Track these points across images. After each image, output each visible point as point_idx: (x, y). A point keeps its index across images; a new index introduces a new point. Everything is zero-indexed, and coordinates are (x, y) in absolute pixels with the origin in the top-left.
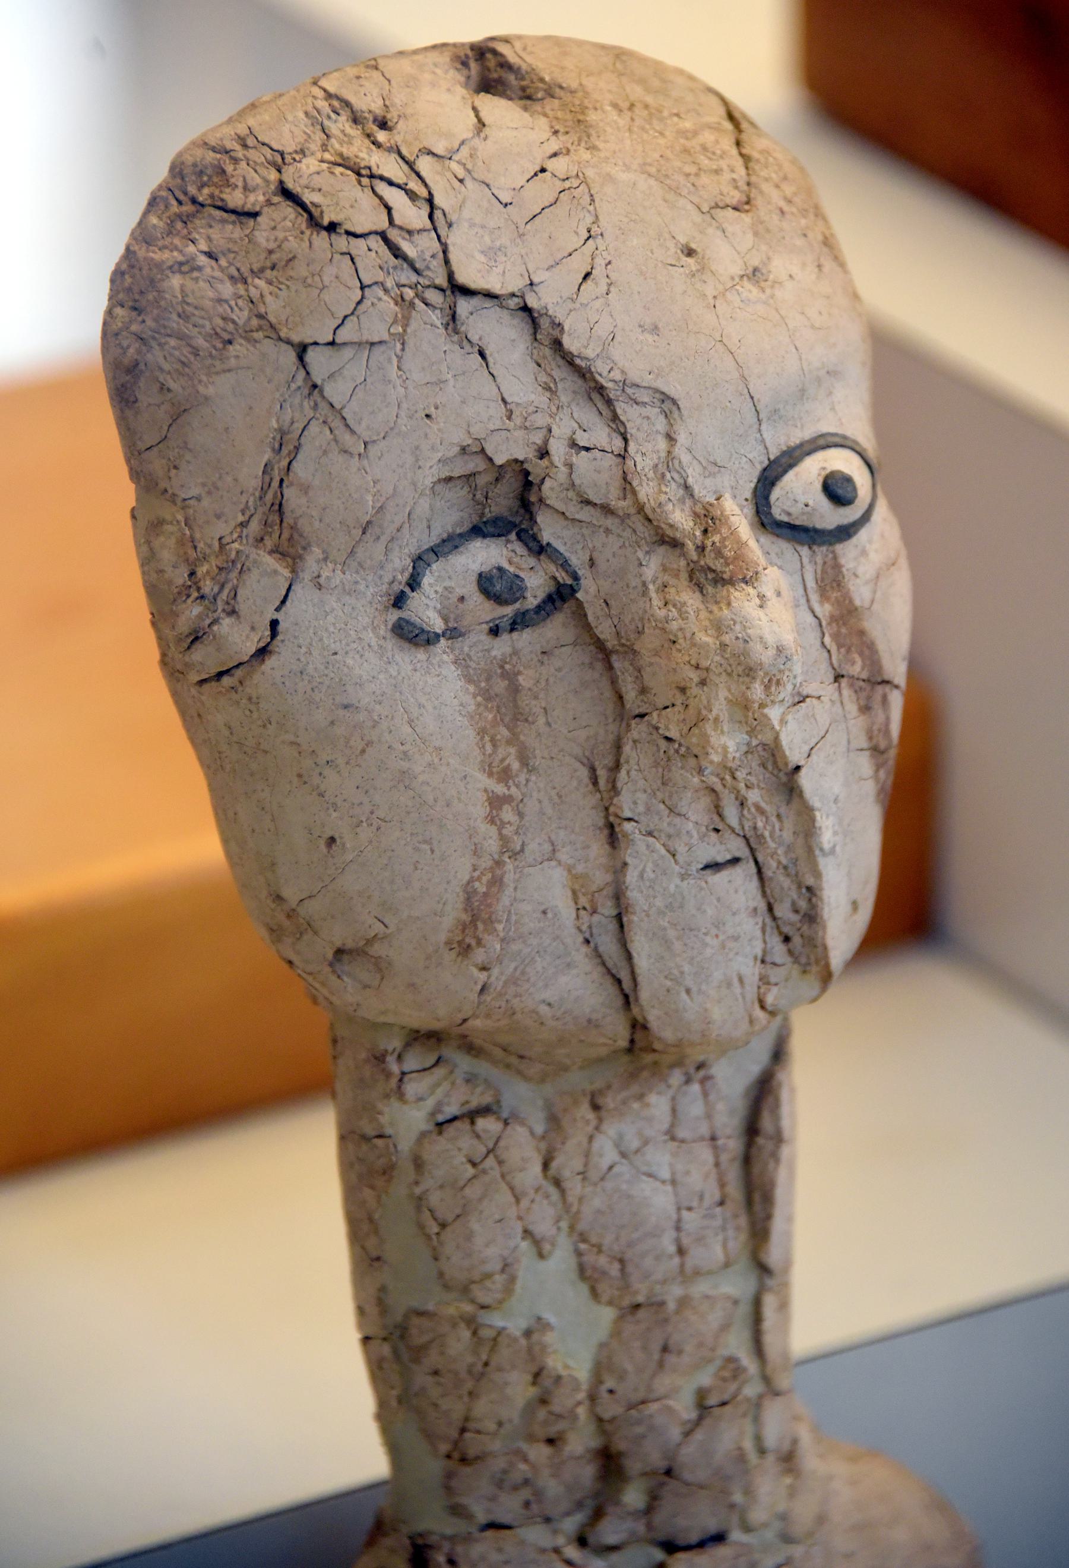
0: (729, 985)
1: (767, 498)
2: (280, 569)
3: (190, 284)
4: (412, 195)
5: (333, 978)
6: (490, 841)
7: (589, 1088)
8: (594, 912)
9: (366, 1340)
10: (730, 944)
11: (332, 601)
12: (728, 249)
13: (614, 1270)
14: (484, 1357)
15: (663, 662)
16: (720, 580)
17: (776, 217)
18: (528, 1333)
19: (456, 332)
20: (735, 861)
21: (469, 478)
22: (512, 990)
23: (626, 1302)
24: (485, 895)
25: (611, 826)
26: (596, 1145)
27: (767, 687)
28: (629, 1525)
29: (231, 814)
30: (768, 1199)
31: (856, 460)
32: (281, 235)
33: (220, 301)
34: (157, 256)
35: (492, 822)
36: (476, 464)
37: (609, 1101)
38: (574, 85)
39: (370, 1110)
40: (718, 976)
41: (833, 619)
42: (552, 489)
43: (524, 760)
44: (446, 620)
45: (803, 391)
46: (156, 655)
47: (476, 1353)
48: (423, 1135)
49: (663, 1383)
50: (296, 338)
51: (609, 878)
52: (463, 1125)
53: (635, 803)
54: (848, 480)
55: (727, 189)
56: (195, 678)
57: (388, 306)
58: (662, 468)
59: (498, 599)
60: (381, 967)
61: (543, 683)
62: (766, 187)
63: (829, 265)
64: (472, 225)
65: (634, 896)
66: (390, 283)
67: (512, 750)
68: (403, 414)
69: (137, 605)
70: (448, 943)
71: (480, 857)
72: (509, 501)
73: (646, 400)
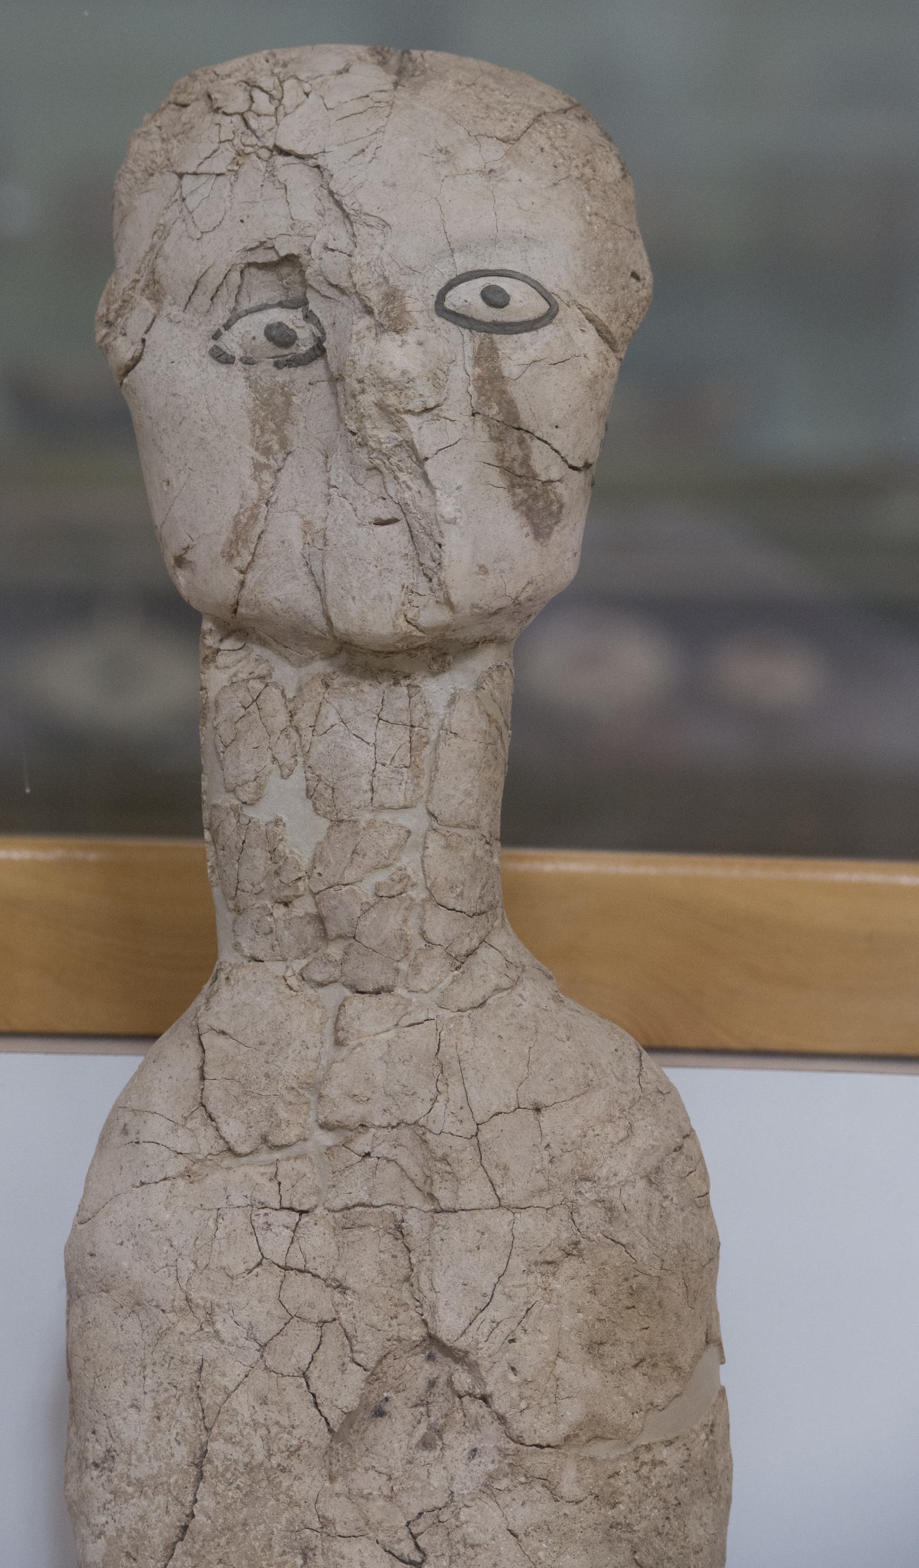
2: (150, 307)
6: (252, 491)
14: (243, 837)
24: (246, 524)
35: (255, 479)
37: (336, 683)
42: (311, 274)
50: (179, 171)
53: (338, 476)
61: (307, 402)
67: (275, 438)
68: (226, 218)
71: (245, 500)
73: (373, 224)
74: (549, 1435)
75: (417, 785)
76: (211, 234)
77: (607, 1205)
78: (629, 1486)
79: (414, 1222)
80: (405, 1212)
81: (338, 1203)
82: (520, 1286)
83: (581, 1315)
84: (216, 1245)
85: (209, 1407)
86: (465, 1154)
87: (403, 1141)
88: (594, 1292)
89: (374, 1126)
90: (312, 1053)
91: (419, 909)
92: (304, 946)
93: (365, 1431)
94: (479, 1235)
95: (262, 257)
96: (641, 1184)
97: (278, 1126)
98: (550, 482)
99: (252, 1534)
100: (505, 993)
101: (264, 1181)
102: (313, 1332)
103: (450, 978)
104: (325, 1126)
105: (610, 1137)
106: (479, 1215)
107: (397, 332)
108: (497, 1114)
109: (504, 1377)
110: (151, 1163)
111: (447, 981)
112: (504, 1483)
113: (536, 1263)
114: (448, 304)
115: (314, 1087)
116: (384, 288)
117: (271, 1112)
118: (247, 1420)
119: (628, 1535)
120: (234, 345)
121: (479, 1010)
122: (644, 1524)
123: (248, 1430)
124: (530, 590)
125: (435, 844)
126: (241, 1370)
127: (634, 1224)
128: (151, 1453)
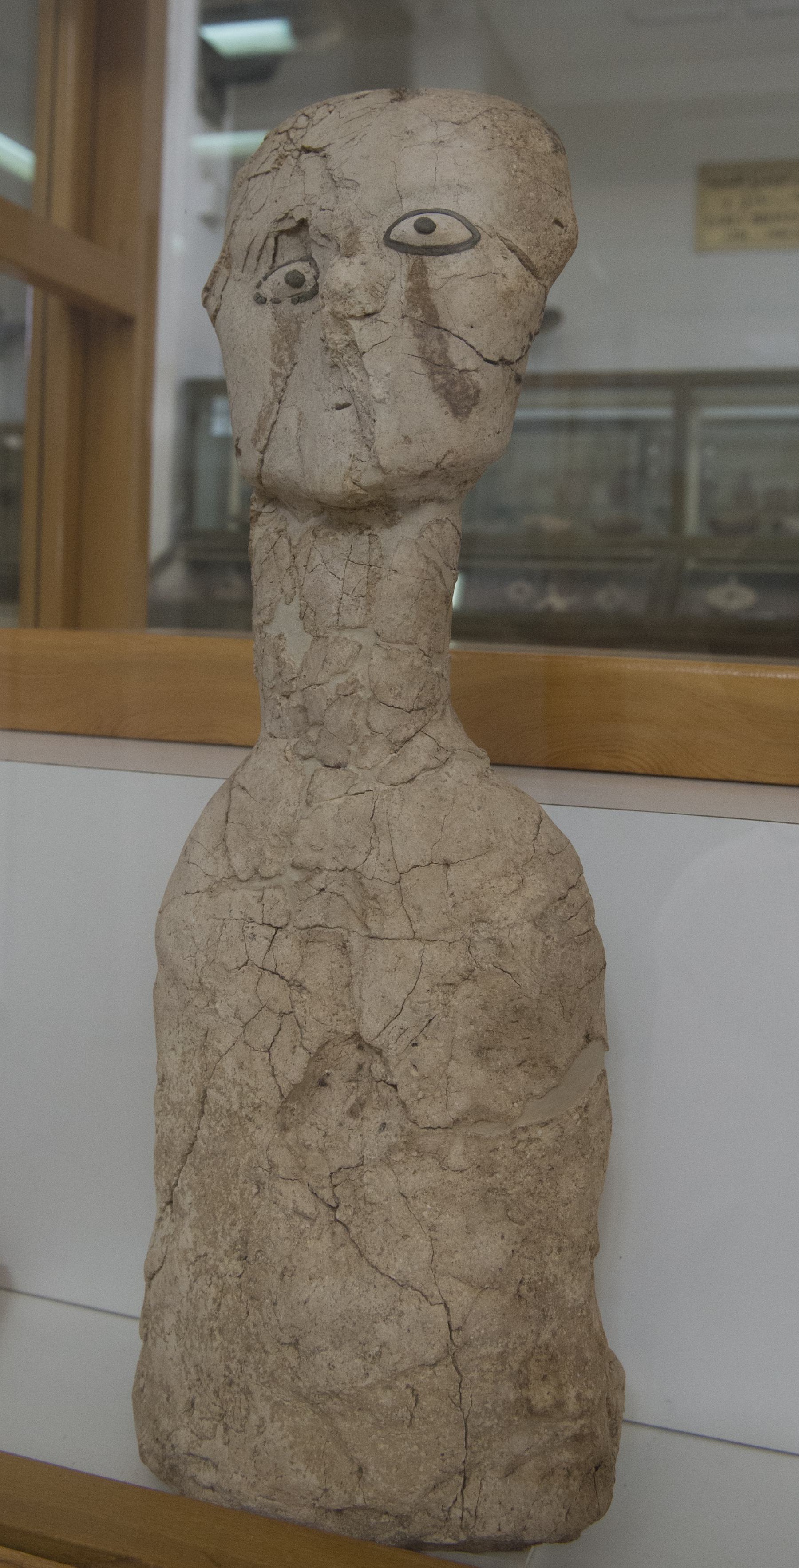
74: (439, 1119)
75: (369, 610)
77: (498, 942)
78: (506, 1160)
79: (355, 943)
80: (349, 934)
81: (302, 924)
82: (424, 1002)
83: (472, 1027)
84: (219, 946)
86: (390, 896)
87: (347, 882)
88: (485, 1008)
89: (325, 869)
90: (291, 810)
91: (365, 705)
92: (297, 729)
93: (313, 1095)
94: (396, 959)
95: (288, 225)
96: (528, 926)
97: (264, 862)
98: (466, 371)
100: (433, 771)
101: (253, 902)
102: (275, 1019)
103: (389, 758)
104: (294, 866)
105: (504, 889)
106: (398, 944)
107: (348, 257)
108: (415, 867)
109: (407, 1072)
111: (386, 762)
112: (400, 1156)
113: (438, 985)
114: (392, 237)
115: (289, 834)
116: (350, 230)
117: (261, 853)
119: (503, 1197)
120: (267, 290)
121: (408, 785)
122: (518, 1188)
124: (450, 458)
125: (378, 656)
126: (230, 1039)
127: (520, 958)
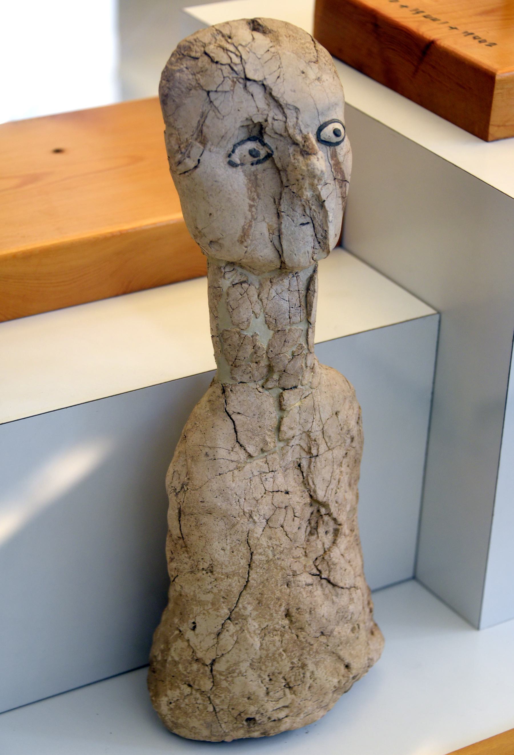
0: (305, 253)
1: (320, 134)
3: (181, 75)
4: (237, 55)
5: (209, 248)
7: (270, 277)
8: (273, 234)
9: (213, 336)
10: (306, 243)
11: (213, 155)
12: (312, 72)
13: (274, 322)
15: (293, 173)
16: (308, 154)
17: (324, 65)
18: (252, 336)
19: (246, 89)
20: (308, 223)
21: (248, 126)
22: (253, 252)
23: (276, 330)
24: (248, 229)
25: (278, 213)
26: (271, 291)
27: (318, 181)
28: (275, 383)
29: (186, 207)
30: (311, 306)
31: (341, 126)
32: (204, 63)
33: (189, 79)
34: (174, 68)
36: (249, 123)
37: (274, 281)
38: (276, 30)
39: (217, 281)
40: (302, 251)
41: (334, 165)
43: (258, 196)
44: (241, 161)
45: (329, 108)
46: (169, 167)
47: (240, 341)
48: (229, 287)
49: (284, 350)
50: (207, 89)
51: (277, 226)
52: (239, 285)
54: (339, 130)
55: (312, 57)
56: (179, 173)
57: (230, 82)
58: (295, 125)
59: (254, 156)
60: (221, 246)
62: (322, 58)
63: (336, 78)
64: (251, 63)
65: (283, 230)
66: (231, 77)
67: (255, 194)
69: (165, 155)
70: (238, 241)
72: (257, 132)
76: (227, 117)
84: (251, 491)
85: (252, 545)
97: (267, 444)
99: (271, 582)
110: (222, 466)
118: (266, 546)
123: (266, 549)
128: (231, 564)
